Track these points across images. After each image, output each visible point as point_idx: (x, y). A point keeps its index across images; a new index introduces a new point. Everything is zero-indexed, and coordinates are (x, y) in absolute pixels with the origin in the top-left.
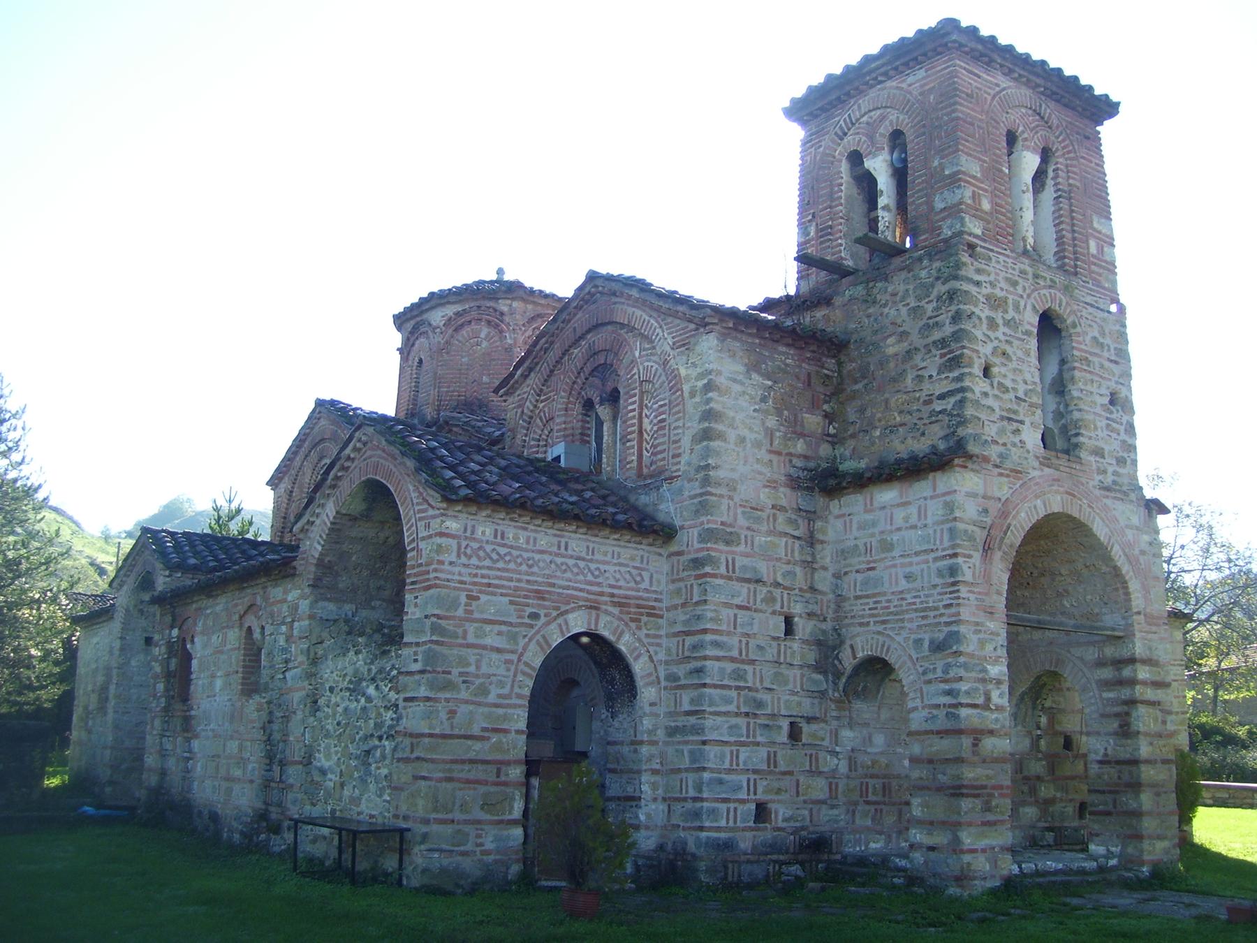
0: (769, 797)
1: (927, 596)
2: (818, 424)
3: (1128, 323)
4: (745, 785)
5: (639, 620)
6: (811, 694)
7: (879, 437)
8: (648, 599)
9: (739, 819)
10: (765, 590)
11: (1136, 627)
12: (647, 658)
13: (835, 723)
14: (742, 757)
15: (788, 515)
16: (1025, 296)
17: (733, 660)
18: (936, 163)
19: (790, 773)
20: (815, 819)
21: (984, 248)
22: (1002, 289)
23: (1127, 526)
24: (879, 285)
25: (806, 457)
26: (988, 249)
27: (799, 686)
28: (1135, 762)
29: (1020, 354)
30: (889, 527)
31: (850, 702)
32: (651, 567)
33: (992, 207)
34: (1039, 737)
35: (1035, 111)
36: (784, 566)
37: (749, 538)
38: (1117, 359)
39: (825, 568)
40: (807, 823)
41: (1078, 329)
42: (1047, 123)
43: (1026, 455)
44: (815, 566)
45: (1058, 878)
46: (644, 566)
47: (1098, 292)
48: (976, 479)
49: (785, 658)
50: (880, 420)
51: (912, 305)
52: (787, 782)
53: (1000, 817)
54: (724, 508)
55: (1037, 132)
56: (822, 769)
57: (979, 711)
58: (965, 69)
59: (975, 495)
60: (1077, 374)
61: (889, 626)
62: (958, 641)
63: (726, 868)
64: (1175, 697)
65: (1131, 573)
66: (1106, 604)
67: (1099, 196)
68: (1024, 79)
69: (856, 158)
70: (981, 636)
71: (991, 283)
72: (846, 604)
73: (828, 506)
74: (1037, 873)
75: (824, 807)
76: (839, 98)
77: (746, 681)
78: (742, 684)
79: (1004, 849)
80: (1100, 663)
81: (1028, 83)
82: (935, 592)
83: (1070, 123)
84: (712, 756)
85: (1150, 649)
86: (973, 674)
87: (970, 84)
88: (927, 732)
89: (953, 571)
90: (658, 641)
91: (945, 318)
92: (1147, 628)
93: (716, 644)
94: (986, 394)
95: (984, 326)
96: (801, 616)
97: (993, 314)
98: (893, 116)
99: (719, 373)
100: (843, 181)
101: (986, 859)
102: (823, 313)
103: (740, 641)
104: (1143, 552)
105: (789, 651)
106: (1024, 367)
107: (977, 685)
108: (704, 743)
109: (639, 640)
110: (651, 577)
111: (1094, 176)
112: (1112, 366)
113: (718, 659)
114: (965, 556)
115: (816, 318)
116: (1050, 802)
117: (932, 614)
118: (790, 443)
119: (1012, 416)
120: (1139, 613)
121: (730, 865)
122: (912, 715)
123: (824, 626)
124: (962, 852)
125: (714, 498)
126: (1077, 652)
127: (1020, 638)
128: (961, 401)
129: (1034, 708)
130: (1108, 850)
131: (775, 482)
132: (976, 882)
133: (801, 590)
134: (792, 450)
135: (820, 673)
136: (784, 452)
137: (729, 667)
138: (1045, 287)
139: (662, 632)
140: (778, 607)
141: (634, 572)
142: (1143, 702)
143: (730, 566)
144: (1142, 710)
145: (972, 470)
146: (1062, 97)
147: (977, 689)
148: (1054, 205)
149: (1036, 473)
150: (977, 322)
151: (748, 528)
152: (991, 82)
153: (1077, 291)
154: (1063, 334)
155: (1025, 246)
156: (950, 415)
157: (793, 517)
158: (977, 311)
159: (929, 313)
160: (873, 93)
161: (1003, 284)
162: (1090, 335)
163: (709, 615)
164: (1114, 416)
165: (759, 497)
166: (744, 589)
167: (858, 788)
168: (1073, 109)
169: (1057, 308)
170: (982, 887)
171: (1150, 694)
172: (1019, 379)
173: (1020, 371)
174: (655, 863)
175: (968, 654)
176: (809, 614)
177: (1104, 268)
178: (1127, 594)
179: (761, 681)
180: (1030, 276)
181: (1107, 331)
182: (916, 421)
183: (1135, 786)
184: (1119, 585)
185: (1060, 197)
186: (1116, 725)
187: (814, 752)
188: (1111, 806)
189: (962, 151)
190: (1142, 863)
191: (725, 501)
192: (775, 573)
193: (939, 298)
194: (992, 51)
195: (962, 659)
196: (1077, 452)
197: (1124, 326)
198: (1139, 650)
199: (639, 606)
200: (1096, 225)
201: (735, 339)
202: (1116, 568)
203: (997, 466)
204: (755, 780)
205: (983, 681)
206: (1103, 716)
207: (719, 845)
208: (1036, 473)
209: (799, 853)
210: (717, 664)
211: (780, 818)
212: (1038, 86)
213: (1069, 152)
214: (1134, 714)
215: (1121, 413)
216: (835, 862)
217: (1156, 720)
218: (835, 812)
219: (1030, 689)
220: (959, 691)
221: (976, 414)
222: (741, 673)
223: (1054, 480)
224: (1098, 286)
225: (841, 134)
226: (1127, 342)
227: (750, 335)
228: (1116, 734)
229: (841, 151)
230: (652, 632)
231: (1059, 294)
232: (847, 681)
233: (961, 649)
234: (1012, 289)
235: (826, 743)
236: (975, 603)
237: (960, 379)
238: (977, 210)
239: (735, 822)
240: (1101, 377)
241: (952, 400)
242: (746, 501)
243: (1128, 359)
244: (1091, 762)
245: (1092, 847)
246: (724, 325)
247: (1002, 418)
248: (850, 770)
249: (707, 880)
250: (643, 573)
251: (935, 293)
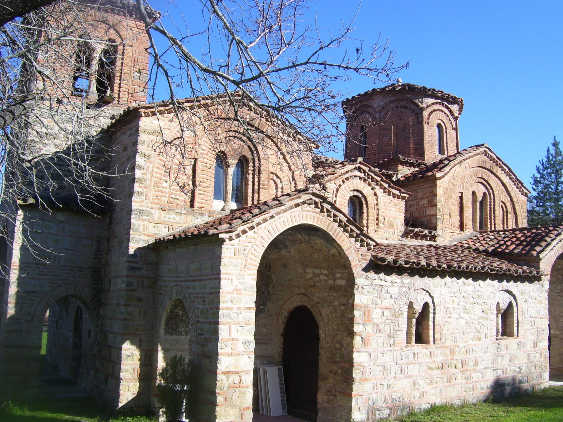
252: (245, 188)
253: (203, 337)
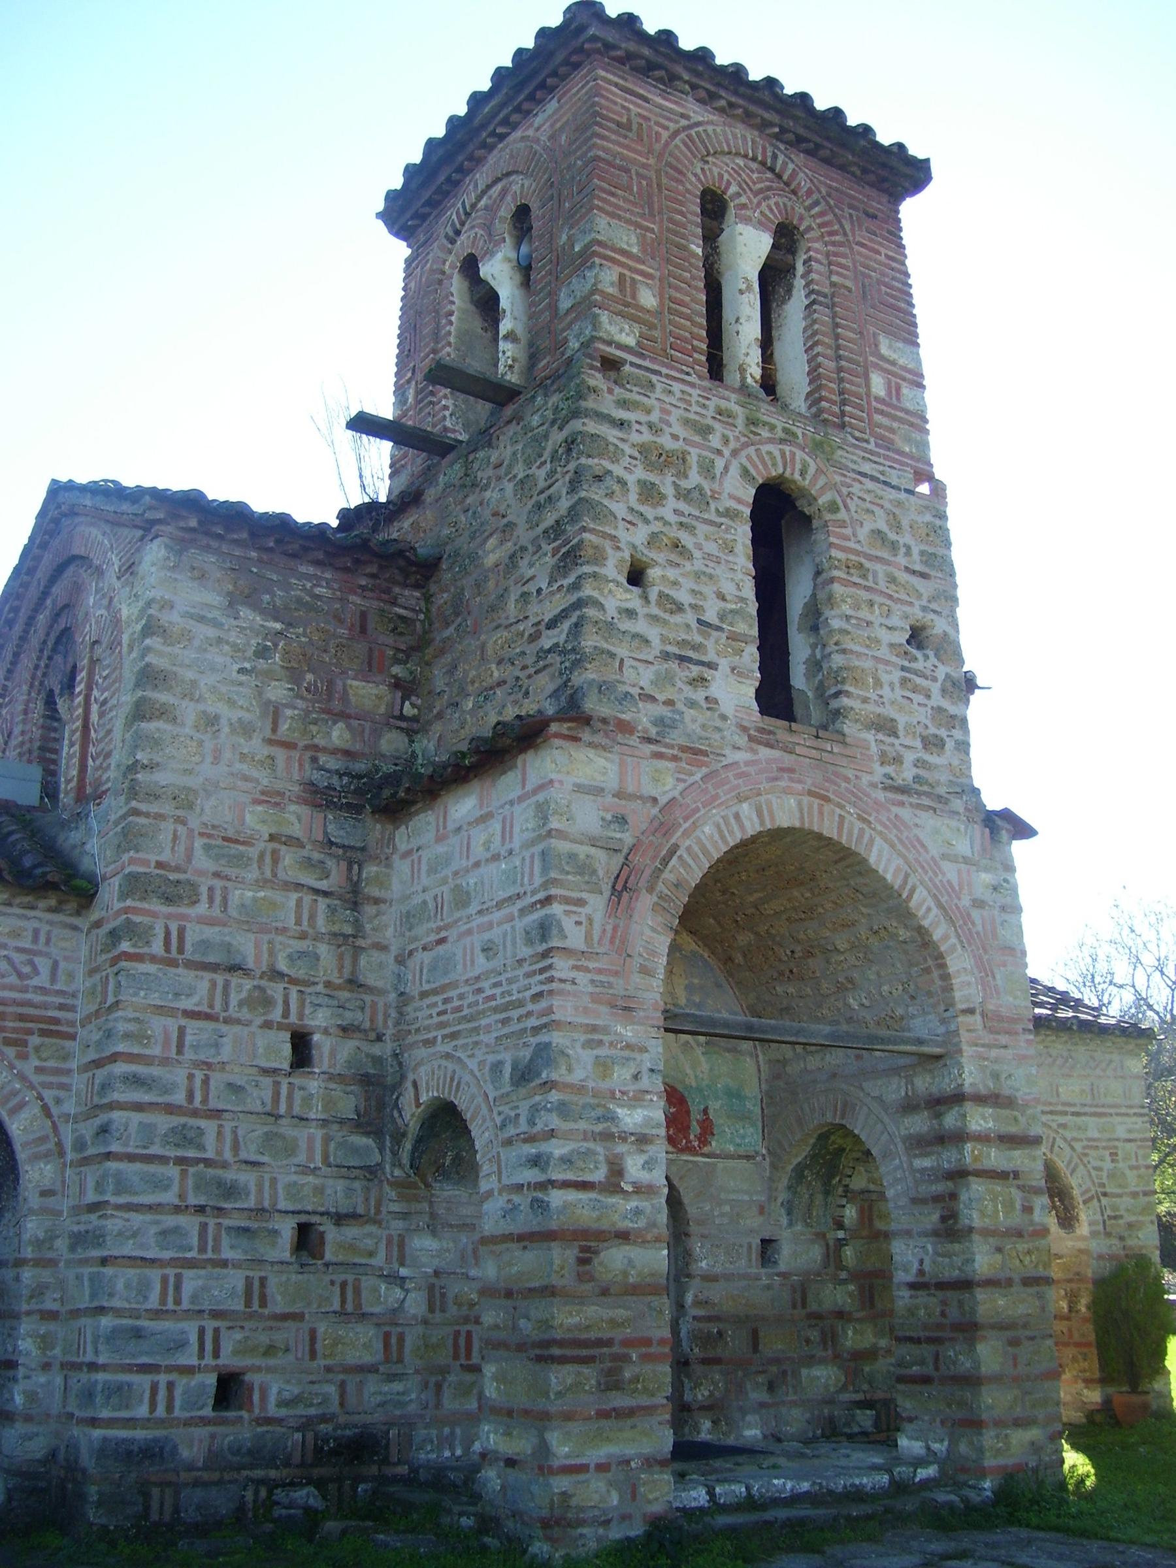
0: (247, 1361)
1: (510, 981)
2: (379, 697)
3: (950, 511)
4: (193, 1338)
5: (25, 1043)
6: (345, 1171)
7: (472, 712)
8: (45, 1006)
9: (178, 1403)
10: (248, 984)
11: (965, 1036)
12: (37, 1110)
13: (398, 1225)
14: (188, 1288)
15: (305, 853)
16: (727, 452)
17: (170, 1109)
19: (298, 1317)
20: (351, 1400)
21: (639, 367)
22: (675, 437)
23: (944, 857)
24: (481, 454)
25: (347, 753)
26: (647, 369)
27: (318, 1157)
28: (965, 1285)
29: (711, 548)
31: (428, 1185)
32: (54, 950)
33: (661, 304)
34: (841, 1243)
35: (763, 163)
37: (218, 892)
38: (926, 570)
39: (382, 948)
40: (334, 1407)
41: (842, 515)
42: (787, 184)
43: (719, 723)
44: (361, 942)
45: (782, 1514)
46: (41, 946)
47: (886, 458)
48: (601, 762)
49: (290, 1106)
50: (473, 682)
51: (520, 476)
52: (289, 1333)
53: (644, 1401)
54: (165, 837)
56: (367, 1309)
57: (593, 1195)
58: (616, 85)
59: (598, 791)
62: (550, 1062)
63: (147, 1496)
64: (1131, 1168)
65: (953, 940)
67: (899, 309)
68: (740, 111)
69: (470, 265)
70: (602, 1052)
71: (650, 426)
72: (409, 1009)
73: (391, 839)
74: (750, 1503)
76: (449, 180)
77: (201, 1147)
78: (191, 1153)
79: (650, 1462)
80: (909, 1107)
81: (747, 118)
82: (520, 972)
83: (837, 190)
84: (120, 1285)
85: (996, 1076)
86: (582, 1125)
87: (628, 110)
88: (508, 1238)
89: (544, 929)
90: (64, 1080)
91: (561, 487)
92: (988, 1038)
93: (137, 1081)
94: (631, 613)
95: (633, 497)
96: (326, 1032)
97: (652, 477)
98: (518, 184)
100: (454, 307)
101: (610, 1484)
102: (411, 520)
103: (191, 1077)
104: (979, 904)
105: (298, 1095)
107: (591, 1145)
109: (22, 1077)
110: (55, 965)
111: (883, 274)
112: (915, 581)
113: (138, 1107)
114: (567, 901)
115: (401, 530)
117: (515, 1014)
118: (314, 728)
119: (690, 654)
120: (971, 1011)
121: (155, 1492)
124: (552, 1471)
125: (142, 820)
126: (874, 1087)
127: (788, 1069)
128: (576, 625)
129: (827, 1193)
130: (928, 1448)
131: (280, 794)
133: (328, 984)
134: (320, 741)
135: (367, 1134)
136: (301, 744)
137: (164, 1123)
138: (771, 441)
139: (74, 1065)
140: (276, 1015)
141: (17, 957)
142: (979, 1173)
143: (175, 941)
144: (977, 1187)
145: (591, 745)
146: (818, 146)
147: (589, 1153)
148: (805, 319)
149: (741, 756)
150: (616, 487)
151: (217, 875)
152: (671, 111)
153: (840, 452)
154: (815, 523)
155: (743, 379)
156: (564, 652)
157: (316, 856)
158: (617, 470)
159: (542, 484)
160: (492, 159)
162: (868, 526)
163: (122, 1027)
164: (919, 665)
166: (202, 983)
167: (450, 1341)
168: (843, 168)
169: (797, 476)
170: (599, 1540)
171: (994, 1158)
172: (708, 590)
173: (711, 577)
175: (571, 1086)
176: (344, 1029)
177: (894, 418)
178: (946, 977)
179: (236, 1147)
180: (740, 421)
181: (905, 523)
182: (518, 673)
183: (969, 1329)
184: (930, 962)
185: (814, 302)
186: (935, 1217)
187: (350, 1278)
188: (931, 1367)
190: (982, 1473)
191: (168, 826)
192: (271, 953)
194: (673, 61)
195: (555, 1096)
196: (838, 725)
197: (943, 517)
198: (971, 1076)
199: (22, 1018)
200: (884, 350)
201: (207, 548)
202: (921, 931)
203: (649, 740)
204: (217, 1331)
205: (607, 1136)
206: (915, 1201)
207: (129, 1453)
208: (741, 756)
209: (312, 1466)
210: (136, 1117)
211: (272, 1399)
212: (771, 124)
213: (831, 234)
214: (964, 1197)
215: (933, 660)
216: (396, 1479)
217: (1009, 1205)
218: (398, 1387)
219: (813, 1157)
220: (550, 1156)
222: (191, 1134)
223: (782, 770)
225: (451, 233)
226: (948, 544)
228: (935, 1233)
230: (51, 1064)
231: (799, 454)
232: (415, 1149)
233: (554, 1076)
234: (697, 439)
235: (379, 1260)
236: (591, 989)
237: (576, 586)
238: (627, 305)
239: (170, 1407)
240: (890, 597)
241: (566, 625)
242: (214, 827)
243: (949, 571)
244: (899, 1285)
245: (903, 1442)
246: (182, 524)
247: (666, 656)
248: (431, 1309)
249: (104, 1521)
250: (37, 960)
251: (550, 446)
252: (25, 585)
253: (1121, 1222)
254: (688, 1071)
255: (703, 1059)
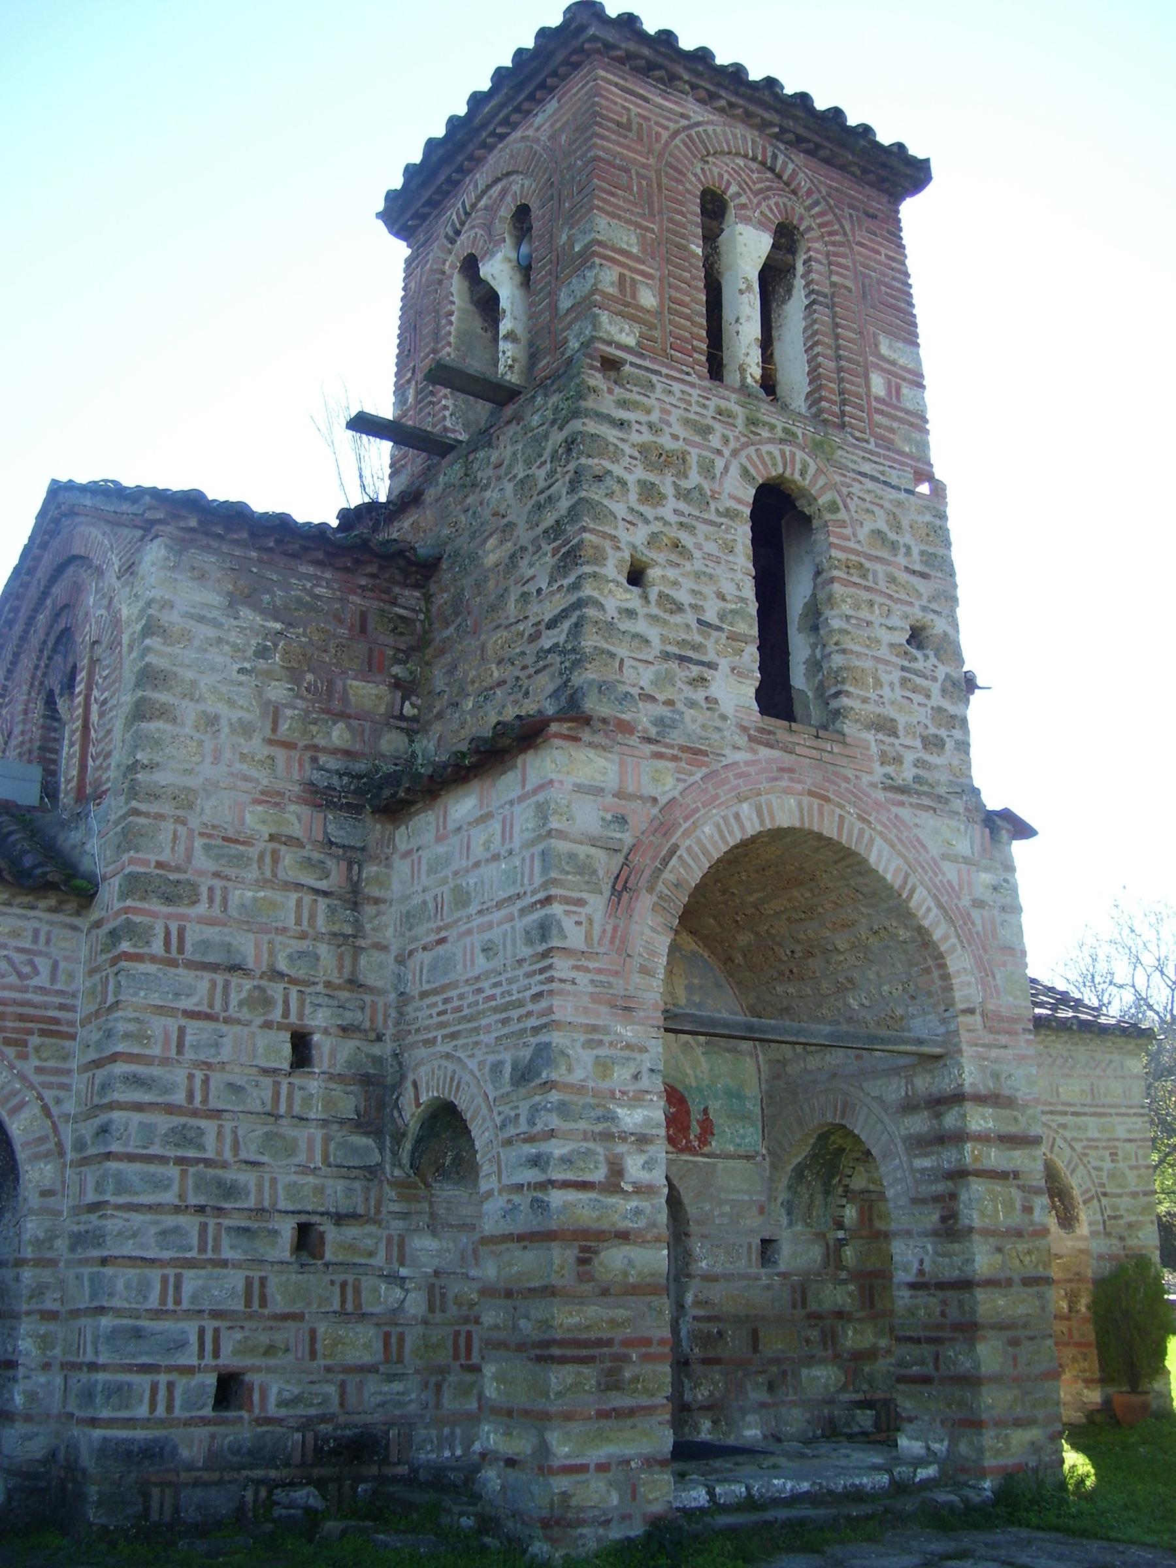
0: (247, 1362)
1: (510, 981)
4: (193, 1338)
6: (345, 1171)
8: (45, 1006)
10: (248, 984)
11: (964, 1036)
12: (37, 1110)
13: (397, 1225)
14: (188, 1288)
15: (305, 853)
16: (727, 453)
17: (170, 1109)
18: (564, 237)
19: (298, 1317)
20: (351, 1400)
21: (639, 367)
22: (675, 437)
23: (944, 857)
24: (481, 454)
25: (347, 753)
26: (647, 369)
27: (318, 1157)
28: (966, 1285)
29: (711, 548)
30: (464, 863)
31: (428, 1185)
32: (54, 951)
33: (661, 304)
34: (841, 1243)
35: (763, 163)
36: (292, 942)
39: (383, 948)
40: (334, 1407)
41: (842, 515)
42: (787, 184)
44: (360, 942)
45: (783, 1514)
46: (41, 946)
47: (886, 458)
48: (601, 762)
49: (290, 1106)
50: (473, 682)
51: (520, 476)
52: (289, 1333)
53: (644, 1401)
54: (165, 837)
55: (768, 198)
56: (367, 1309)
57: (593, 1195)
58: (616, 85)
59: (598, 791)
60: (837, 588)
61: (460, 1042)
62: (550, 1062)
63: (146, 1495)
65: (953, 940)
66: (913, 998)
67: (899, 310)
68: (740, 111)
69: (470, 266)
70: (603, 1052)
71: (650, 426)
73: (391, 839)
74: (750, 1503)
75: (372, 1378)
76: (449, 180)
77: (201, 1147)
78: (191, 1153)
79: (650, 1462)
80: (909, 1107)
81: (747, 118)
83: (837, 190)
84: (120, 1285)
85: (996, 1076)
86: (582, 1125)
87: (628, 110)
89: (544, 929)
90: (64, 1079)
91: (561, 487)
92: (988, 1038)
93: (137, 1081)
94: (631, 613)
95: (633, 497)
96: (326, 1032)
97: (652, 477)
98: (518, 184)
99: (168, 605)
100: (454, 307)
101: (610, 1483)
102: (411, 520)
103: (191, 1077)
104: (979, 904)
105: (298, 1095)
106: (719, 571)
107: (591, 1145)
108: (104, 1261)
109: (22, 1077)
110: (55, 966)
111: (884, 275)
112: (915, 581)
113: (138, 1107)
114: (567, 901)
115: (401, 530)
116: (862, 1356)
117: (515, 1014)
119: (690, 654)
120: (971, 1011)
121: (155, 1492)
122: (487, 1206)
123: (376, 1050)
124: (552, 1471)
125: (142, 820)
126: (874, 1087)
127: (788, 1069)
128: (576, 625)
130: (928, 1448)
131: (280, 794)
132: (585, 1531)
133: (328, 984)
134: (320, 741)
135: (367, 1134)
136: (301, 744)
137: (164, 1123)
138: (771, 441)
140: (277, 1014)
141: (18, 958)
143: (175, 941)
144: (977, 1187)
145: (591, 745)
147: (589, 1153)
148: (805, 318)
151: (217, 875)
152: (671, 111)
153: (840, 452)
154: (815, 523)
155: (743, 379)
156: (564, 652)
157: (316, 856)
158: (617, 470)
159: (542, 484)
160: (492, 159)
161: (678, 429)
162: (868, 526)
164: (919, 665)
165: (242, 821)
166: (202, 983)
167: (450, 1341)
168: (843, 168)
169: (797, 476)
170: (599, 1540)
171: (994, 1158)
173: (711, 577)
174: (42, 1484)
176: (344, 1029)
177: (901, 421)
178: (946, 977)
180: (740, 421)
181: (905, 523)
183: (969, 1329)
184: (930, 962)
185: (814, 302)
186: (936, 1217)
187: (350, 1278)
188: (931, 1366)
189: (600, 209)
191: (168, 826)
192: (271, 953)
193: (554, 457)
194: (673, 61)
195: (555, 1096)
196: (838, 725)
197: (943, 517)
198: (971, 1076)
199: (22, 1018)
200: (884, 350)
201: (207, 548)
202: (921, 931)
203: (649, 740)
204: (217, 1331)
205: (607, 1136)
206: (915, 1201)
207: (129, 1453)
208: (741, 756)
210: (136, 1117)
211: (272, 1399)
212: (771, 124)
213: (831, 234)
214: (964, 1197)
215: (933, 660)
216: (396, 1479)
217: (1009, 1205)
218: (397, 1387)
219: (814, 1156)
220: (550, 1156)
221: (605, 646)
222: (191, 1134)
223: (781, 770)
224: (889, 449)
225: (451, 233)
226: (947, 544)
227: (236, 542)
228: (935, 1233)
229: (451, 264)
230: (51, 1064)
231: (799, 454)
232: (415, 1149)
233: (554, 1076)
234: (697, 439)
235: (379, 1260)
236: (591, 989)
239: (170, 1407)
240: (890, 597)
241: (566, 625)
242: (214, 827)
243: (949, 571)
244: (899, 1285)
245: (903, 1442)
246: (182, 524)
247: (666, 656)
248: (431, 1309)
249: (104, 1521)
250: (37, 960)
251: (549, 446)
253: (1121, 1222)
254: (689, 1071)
255: (703, 1059)
